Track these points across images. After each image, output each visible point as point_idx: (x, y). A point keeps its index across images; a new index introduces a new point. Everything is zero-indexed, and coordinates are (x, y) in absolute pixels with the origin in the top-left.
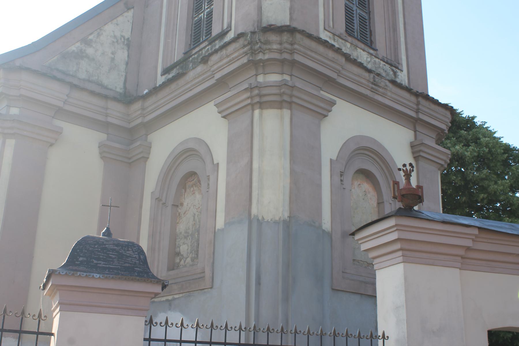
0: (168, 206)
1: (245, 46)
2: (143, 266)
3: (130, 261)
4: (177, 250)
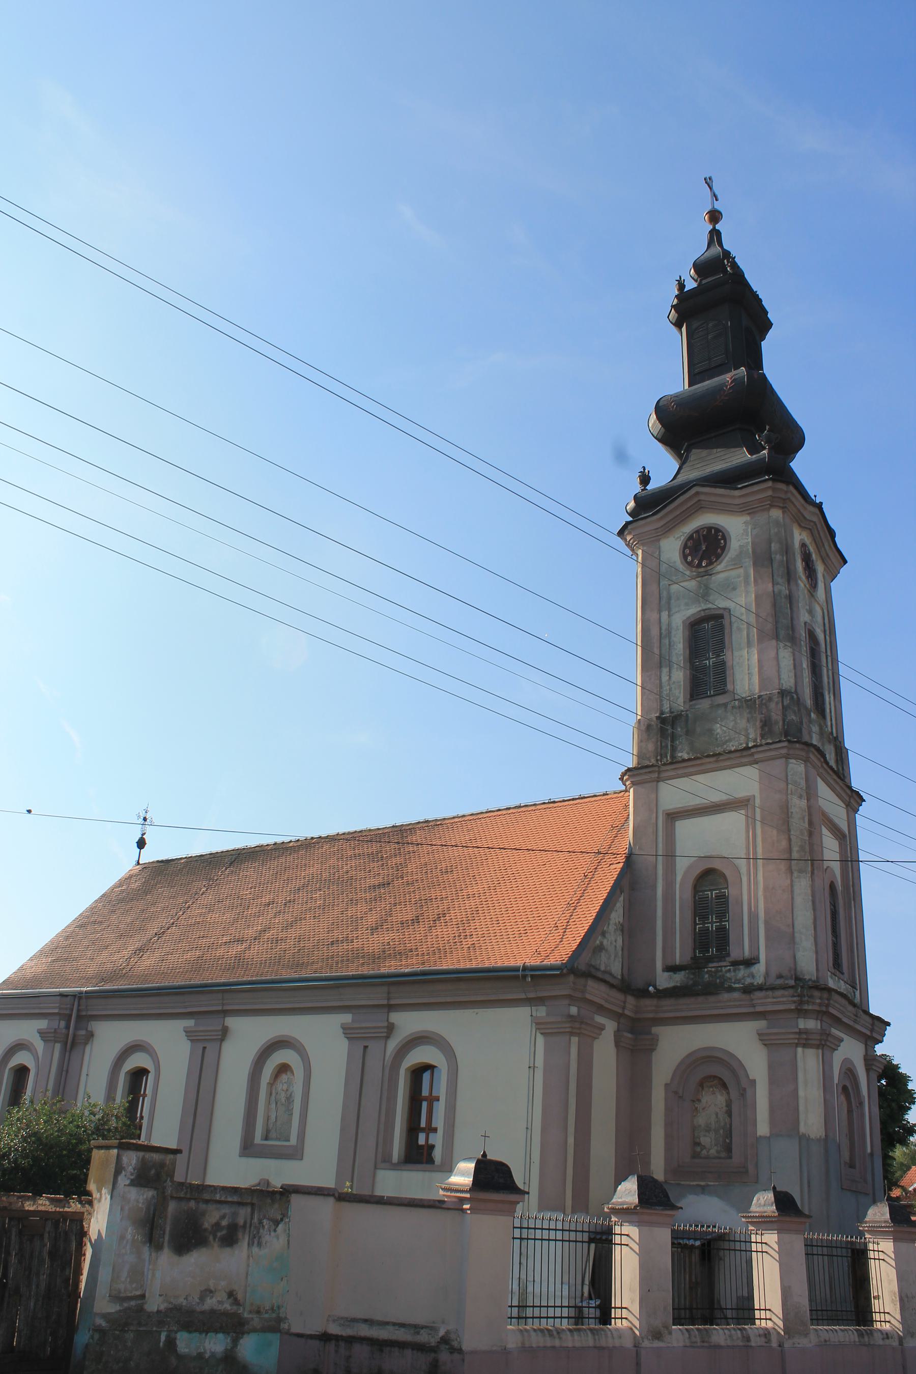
1: (793, 996)
4: (697, 1140)
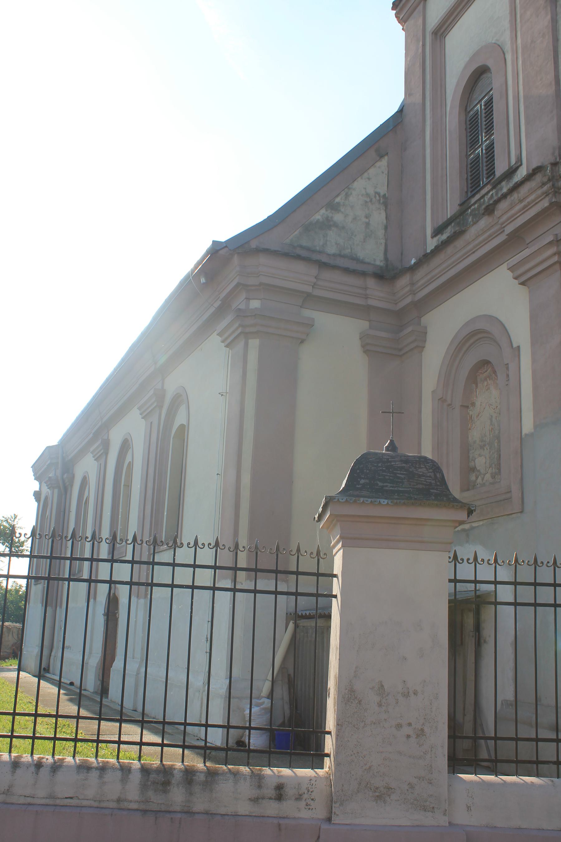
0: (455, 408)
1: (544, 184)
2: (441, 487)
3: (425, 481)
4: (472, 464)
